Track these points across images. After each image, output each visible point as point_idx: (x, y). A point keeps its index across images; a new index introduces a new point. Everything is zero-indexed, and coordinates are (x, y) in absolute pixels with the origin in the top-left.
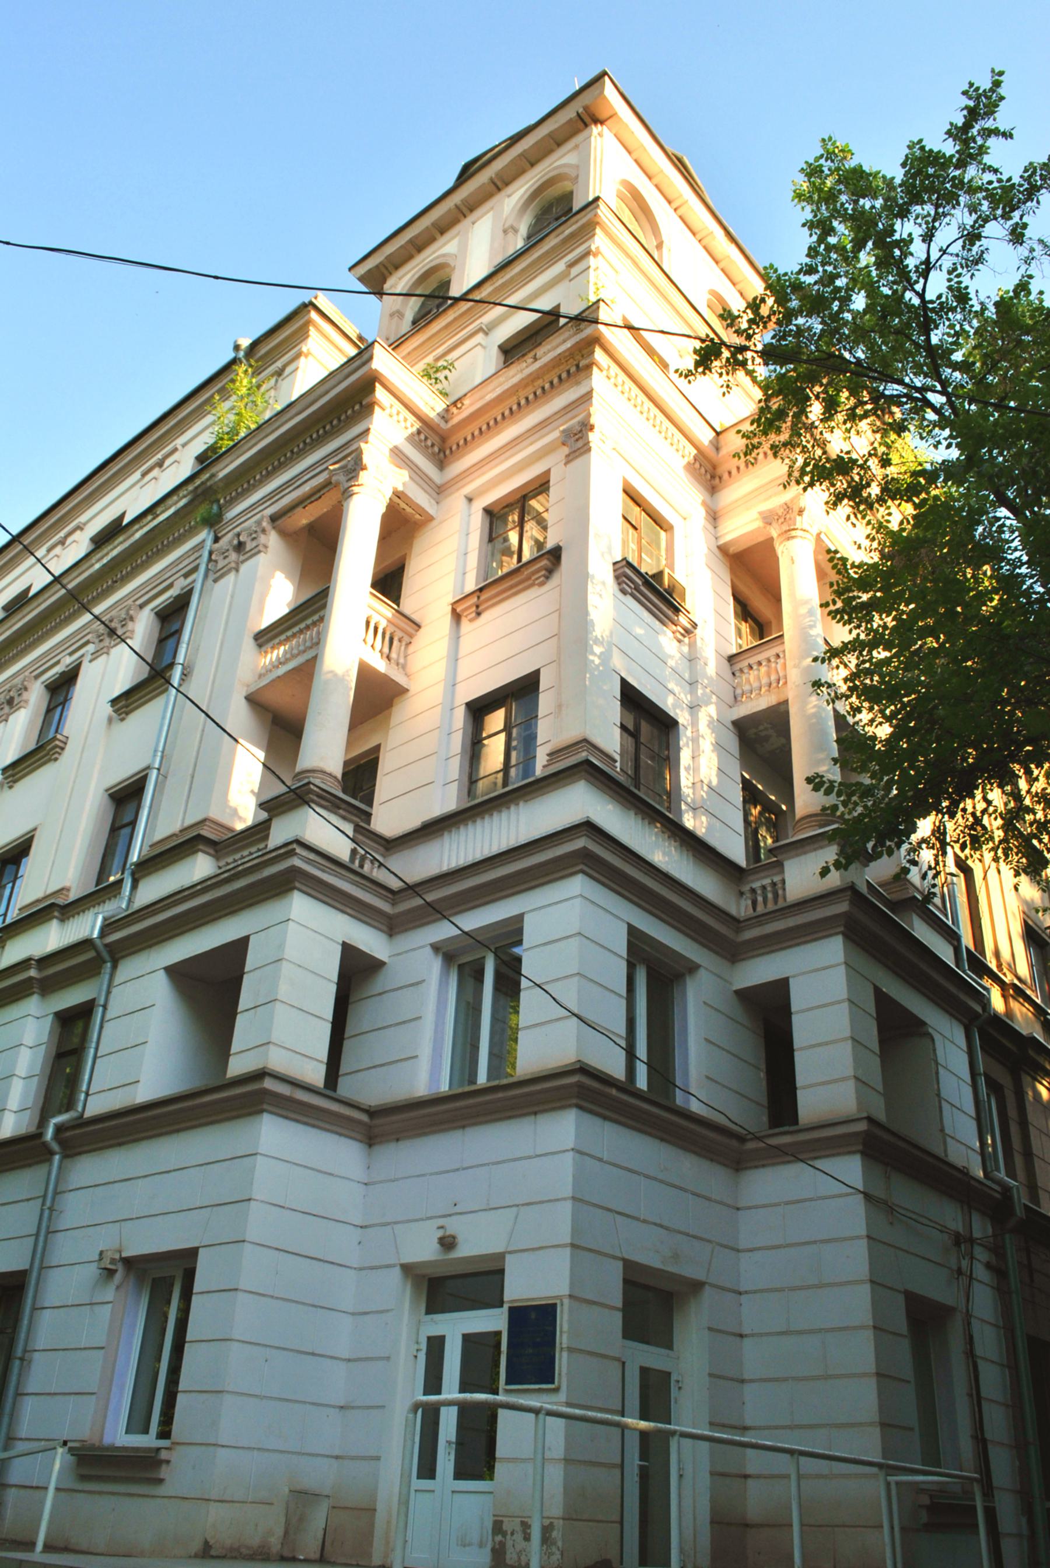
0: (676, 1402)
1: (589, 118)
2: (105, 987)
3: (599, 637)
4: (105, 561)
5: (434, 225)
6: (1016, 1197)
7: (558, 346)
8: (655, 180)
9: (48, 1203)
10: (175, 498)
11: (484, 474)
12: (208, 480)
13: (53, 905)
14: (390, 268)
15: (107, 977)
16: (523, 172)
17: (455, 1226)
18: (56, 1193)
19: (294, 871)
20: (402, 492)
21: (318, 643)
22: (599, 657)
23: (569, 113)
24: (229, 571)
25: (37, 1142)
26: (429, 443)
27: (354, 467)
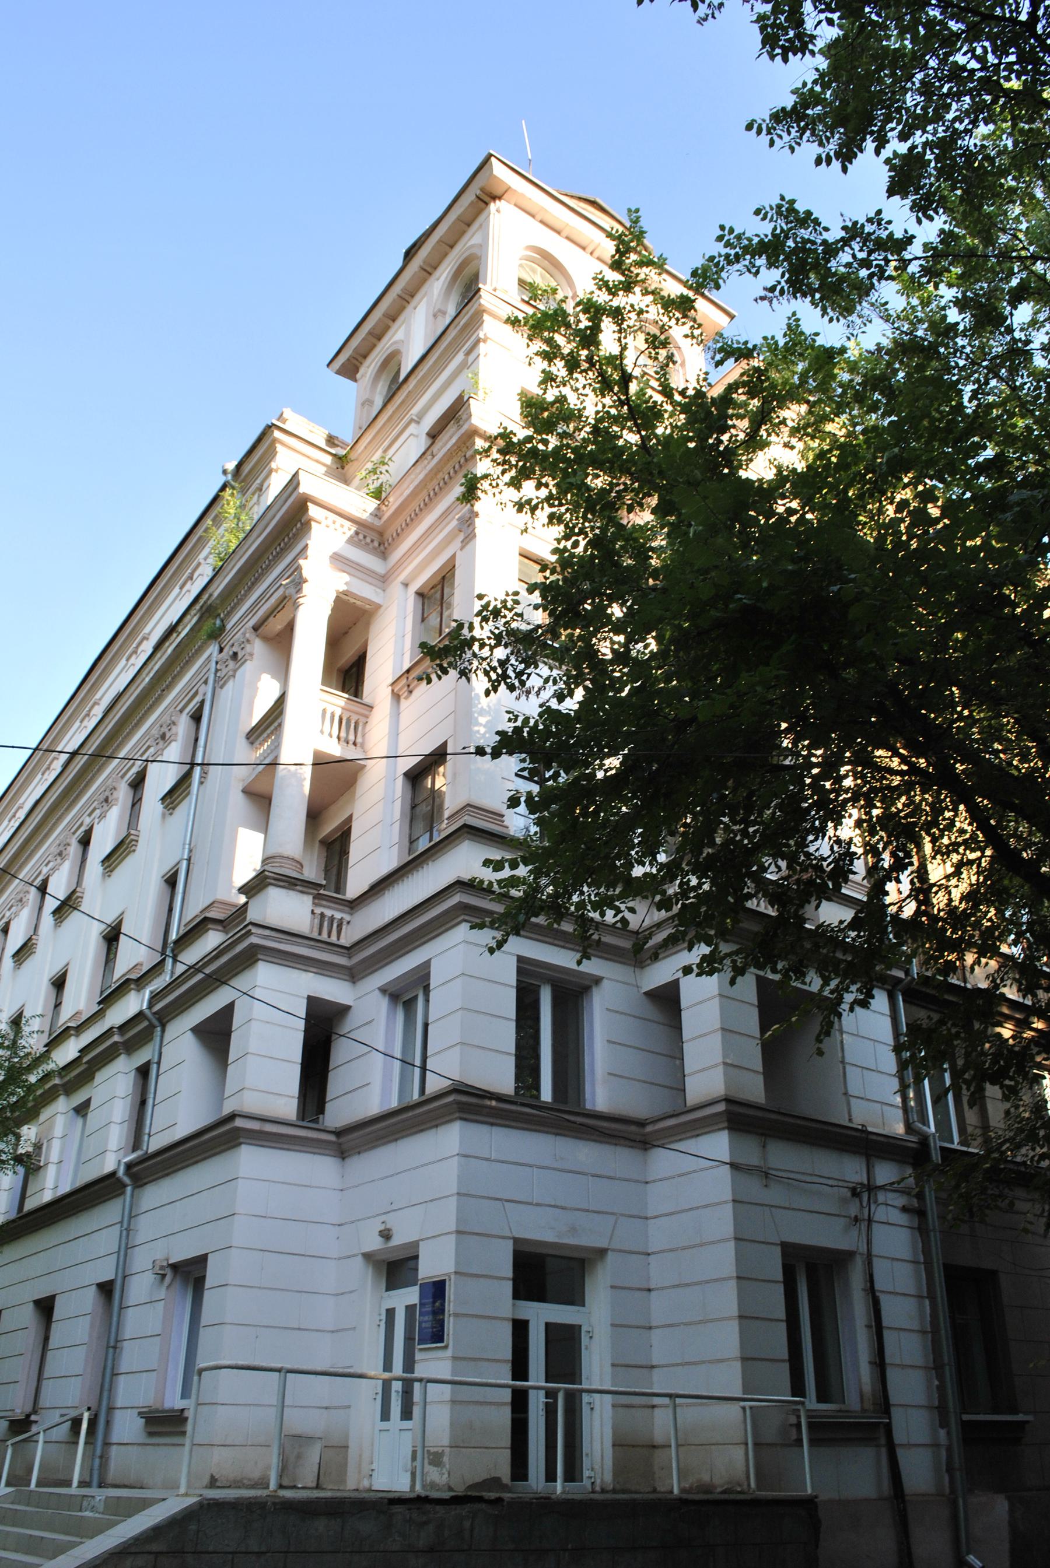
0: (586, 1348)
1: (489, 196)
2: (157, 1048)
3: (485, 707)
4: (151, 675)
5: (386, 315)
6: (932, 1144)
7: (447, 442)
8: (564, 234)
9: (125, 1225)
10: (188, 617)
11: (412, 562)
12: (208, 599)
13: (128, 980)
14: (360, 359)
15: (158, 1038)
16: (446, 255)
17: (393, 1222)
18: (130, 1217)
19: (253, 946)
20: (347, 591)
21: (277, 746)
22: (485, 726)
23: (469, 197)
24: (229, 678)
25: (113, 1180)
26: (368, 540)
27: (299, 582)
